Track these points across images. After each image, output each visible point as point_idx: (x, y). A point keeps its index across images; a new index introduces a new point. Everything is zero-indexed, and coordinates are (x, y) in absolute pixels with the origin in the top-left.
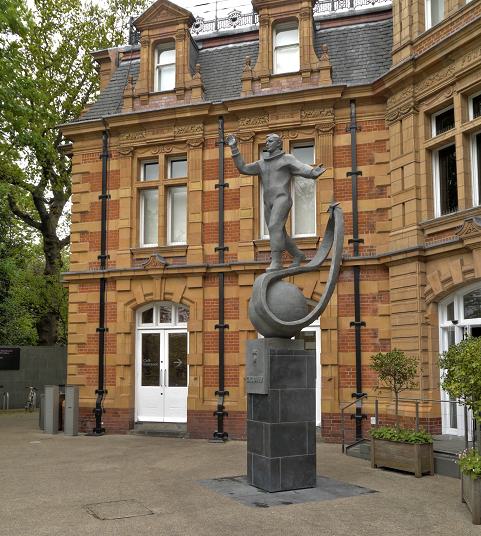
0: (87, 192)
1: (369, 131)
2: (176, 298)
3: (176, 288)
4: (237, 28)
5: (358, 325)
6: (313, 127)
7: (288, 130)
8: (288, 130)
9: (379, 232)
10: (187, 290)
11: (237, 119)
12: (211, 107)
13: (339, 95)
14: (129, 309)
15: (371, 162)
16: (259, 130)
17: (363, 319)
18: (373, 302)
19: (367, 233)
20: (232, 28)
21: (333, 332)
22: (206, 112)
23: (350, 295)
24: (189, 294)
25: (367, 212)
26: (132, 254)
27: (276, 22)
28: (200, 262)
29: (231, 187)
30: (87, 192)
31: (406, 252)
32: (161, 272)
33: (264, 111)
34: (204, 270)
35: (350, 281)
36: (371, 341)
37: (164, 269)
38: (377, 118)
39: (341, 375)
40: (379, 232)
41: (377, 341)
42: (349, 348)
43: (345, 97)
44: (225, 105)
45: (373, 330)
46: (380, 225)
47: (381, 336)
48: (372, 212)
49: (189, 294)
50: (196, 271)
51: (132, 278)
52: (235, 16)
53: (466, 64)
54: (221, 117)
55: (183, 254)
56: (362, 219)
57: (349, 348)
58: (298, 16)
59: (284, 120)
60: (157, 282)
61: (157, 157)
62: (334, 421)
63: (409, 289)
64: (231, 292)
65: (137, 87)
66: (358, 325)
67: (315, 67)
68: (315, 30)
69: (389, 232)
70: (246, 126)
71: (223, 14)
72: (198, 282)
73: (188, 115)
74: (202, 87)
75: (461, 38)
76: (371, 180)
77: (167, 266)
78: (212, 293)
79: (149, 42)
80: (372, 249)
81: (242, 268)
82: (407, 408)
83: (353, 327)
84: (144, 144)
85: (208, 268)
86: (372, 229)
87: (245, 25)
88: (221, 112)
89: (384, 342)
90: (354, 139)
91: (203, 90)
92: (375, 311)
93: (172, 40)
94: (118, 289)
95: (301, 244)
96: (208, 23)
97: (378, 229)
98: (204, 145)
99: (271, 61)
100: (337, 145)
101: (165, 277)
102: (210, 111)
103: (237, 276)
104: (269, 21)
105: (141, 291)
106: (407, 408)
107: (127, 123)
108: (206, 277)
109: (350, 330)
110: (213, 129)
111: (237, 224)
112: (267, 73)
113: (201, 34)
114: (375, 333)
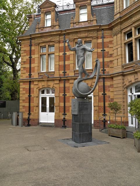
0: (25, 56)
1: (107, 38)
2: (51, 87)
3: (51, 84)
4: (69, 8)
5: (104, 94)
6: (91, 37)
7: (84, 38)
8: (84, 38)
9: (110, 68)
10: (54, 84)
11: (69, 35)
12: (61, 31)
13: (99, 28)
14: (37, 90)
15: (108, 47)
16: (75, 38)
17: (106, 93)
18: (108, 88)
19: (107, 68)
20: (68, 8)
21: (97, 96)
22: (60, 33)
23: (102, 86)
24: (55, 86)
25: (107, 62)
26: (38, 74)
27: (80, 6)
28: (58, 76)
29: (67, 54)
30: (25, 56)
31: (118, 73)
32: (47, 79)
33: (77, 32)
34: (59, 79)
35: (102, 82)
36: (108, 99)
37: (48, 78)
38: (110, 34)
39: (99, 109)
40: (110, 68)
41: (110, 99)
42: (102, 101)
43: (100, 28)
44: (65, 30)
45: (109, 96)
46: (111, 66)
47: (111, 98)
48: (108, 62)
49: (55, 86)
50: (57, 79)
51: (38, 81)
52: (68, 5)
53: (136, 19)
54: (64, 34)
55: (53, 74)
56: (105, 64)
57: (102, 101)
58: (87, 5)
59: (83, 35)
60: (46, 82)
61: (46, 46)
62: (97, 122)
63: (119, 84)
64: (67, 85)
65: (40, 25)
66: (104, 94)
67: (92, 19)
68: (92, 9)
69: (113, 67)
70: (72, 37)
71: (65, 4)
72: (58, 82)
73: (55, 33)
74: (59, 25)
75: (134, 11)
76: (108, 52)
77: (49, 77)
78: (62, 85)
79: (43, 12)
80: (108, 72)
81: (70, 78)
82: (119, 119)
83: (103, 95)
84: (42, 42)
85: (61, 78)
86: (108, 66)
87: (71, 7)
88: (64, 33)
89: (112, 99)
90: (103, 41)
91: (59, 26)
92: (109, 91)
93: (50, 12)
94: (34, 84)
95: (87, 71)
96: (60, 7)
97: (110, 67)
98: (59, 42)
99: (79, 18)
100: (98, 42)
101: (48, 81)
102: (61, 32)
103: (69, 80)
104: (78, 6)
105: (41, 85)
106: (119, 119)
107: (37, 36)
108: (60, 80)
109: (102, 96)
110: (62, 38)
111: (69, 65)
112: (78, 21)
113: (58, 10)
114: (109, 97)
